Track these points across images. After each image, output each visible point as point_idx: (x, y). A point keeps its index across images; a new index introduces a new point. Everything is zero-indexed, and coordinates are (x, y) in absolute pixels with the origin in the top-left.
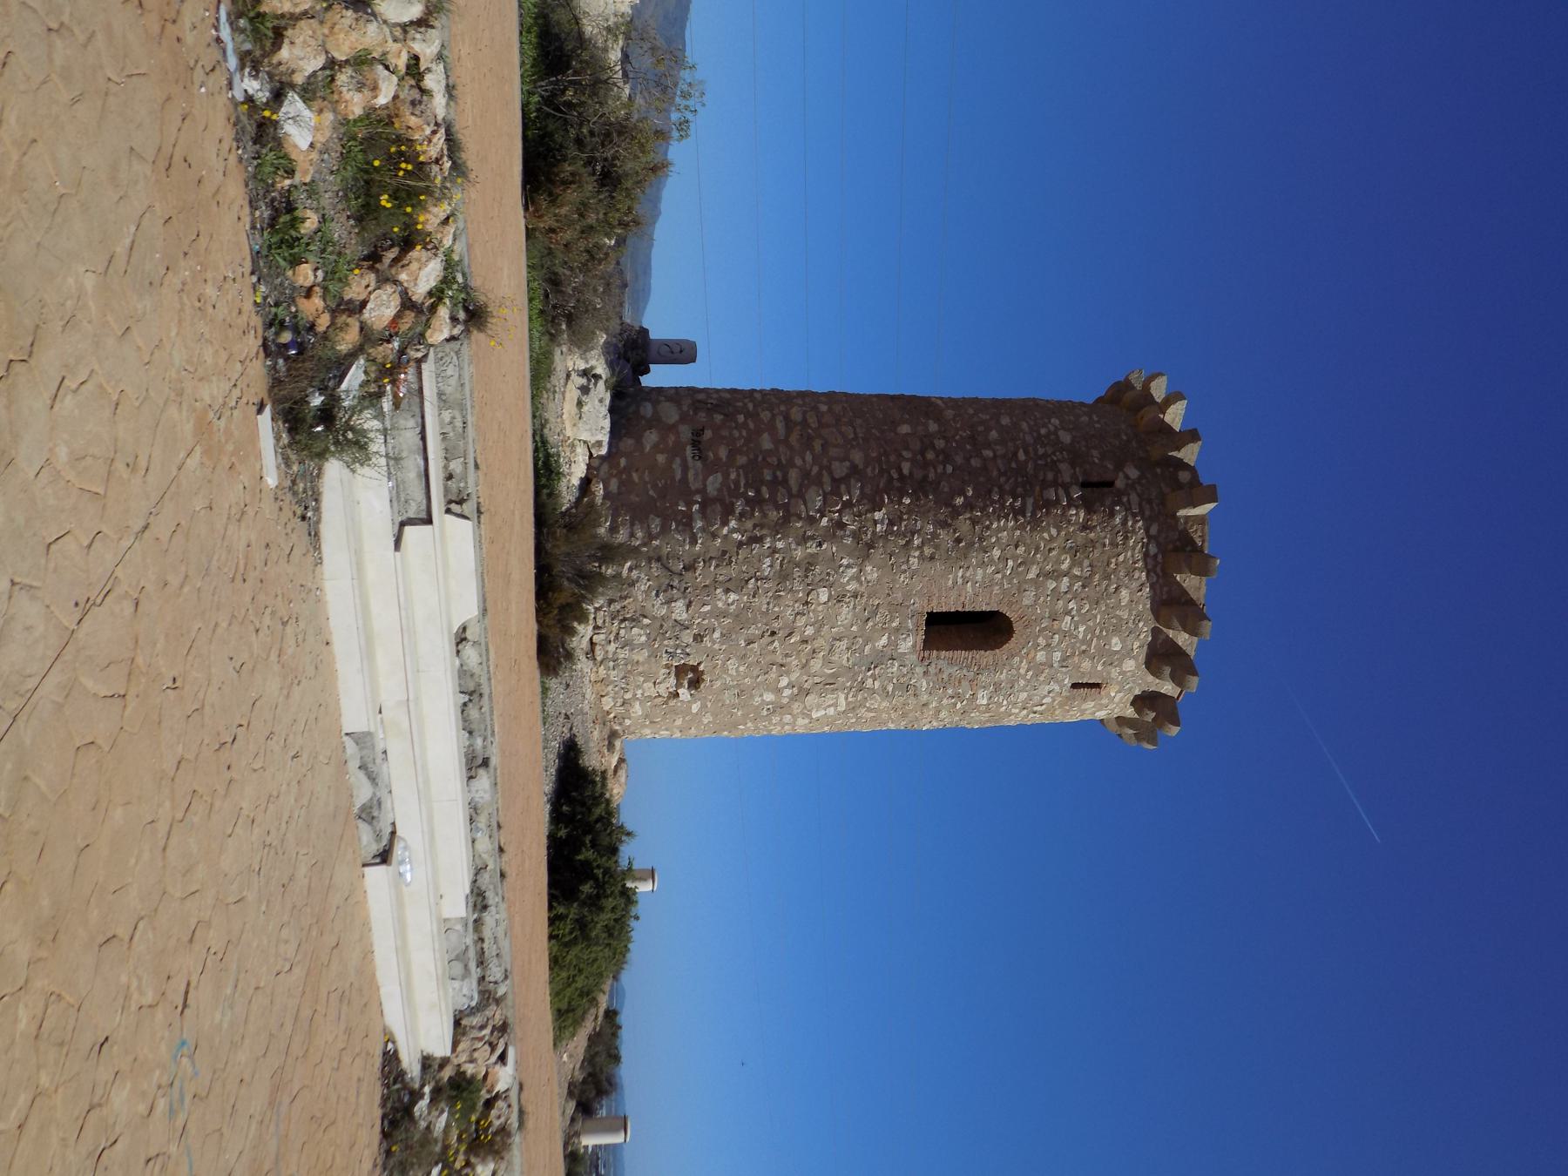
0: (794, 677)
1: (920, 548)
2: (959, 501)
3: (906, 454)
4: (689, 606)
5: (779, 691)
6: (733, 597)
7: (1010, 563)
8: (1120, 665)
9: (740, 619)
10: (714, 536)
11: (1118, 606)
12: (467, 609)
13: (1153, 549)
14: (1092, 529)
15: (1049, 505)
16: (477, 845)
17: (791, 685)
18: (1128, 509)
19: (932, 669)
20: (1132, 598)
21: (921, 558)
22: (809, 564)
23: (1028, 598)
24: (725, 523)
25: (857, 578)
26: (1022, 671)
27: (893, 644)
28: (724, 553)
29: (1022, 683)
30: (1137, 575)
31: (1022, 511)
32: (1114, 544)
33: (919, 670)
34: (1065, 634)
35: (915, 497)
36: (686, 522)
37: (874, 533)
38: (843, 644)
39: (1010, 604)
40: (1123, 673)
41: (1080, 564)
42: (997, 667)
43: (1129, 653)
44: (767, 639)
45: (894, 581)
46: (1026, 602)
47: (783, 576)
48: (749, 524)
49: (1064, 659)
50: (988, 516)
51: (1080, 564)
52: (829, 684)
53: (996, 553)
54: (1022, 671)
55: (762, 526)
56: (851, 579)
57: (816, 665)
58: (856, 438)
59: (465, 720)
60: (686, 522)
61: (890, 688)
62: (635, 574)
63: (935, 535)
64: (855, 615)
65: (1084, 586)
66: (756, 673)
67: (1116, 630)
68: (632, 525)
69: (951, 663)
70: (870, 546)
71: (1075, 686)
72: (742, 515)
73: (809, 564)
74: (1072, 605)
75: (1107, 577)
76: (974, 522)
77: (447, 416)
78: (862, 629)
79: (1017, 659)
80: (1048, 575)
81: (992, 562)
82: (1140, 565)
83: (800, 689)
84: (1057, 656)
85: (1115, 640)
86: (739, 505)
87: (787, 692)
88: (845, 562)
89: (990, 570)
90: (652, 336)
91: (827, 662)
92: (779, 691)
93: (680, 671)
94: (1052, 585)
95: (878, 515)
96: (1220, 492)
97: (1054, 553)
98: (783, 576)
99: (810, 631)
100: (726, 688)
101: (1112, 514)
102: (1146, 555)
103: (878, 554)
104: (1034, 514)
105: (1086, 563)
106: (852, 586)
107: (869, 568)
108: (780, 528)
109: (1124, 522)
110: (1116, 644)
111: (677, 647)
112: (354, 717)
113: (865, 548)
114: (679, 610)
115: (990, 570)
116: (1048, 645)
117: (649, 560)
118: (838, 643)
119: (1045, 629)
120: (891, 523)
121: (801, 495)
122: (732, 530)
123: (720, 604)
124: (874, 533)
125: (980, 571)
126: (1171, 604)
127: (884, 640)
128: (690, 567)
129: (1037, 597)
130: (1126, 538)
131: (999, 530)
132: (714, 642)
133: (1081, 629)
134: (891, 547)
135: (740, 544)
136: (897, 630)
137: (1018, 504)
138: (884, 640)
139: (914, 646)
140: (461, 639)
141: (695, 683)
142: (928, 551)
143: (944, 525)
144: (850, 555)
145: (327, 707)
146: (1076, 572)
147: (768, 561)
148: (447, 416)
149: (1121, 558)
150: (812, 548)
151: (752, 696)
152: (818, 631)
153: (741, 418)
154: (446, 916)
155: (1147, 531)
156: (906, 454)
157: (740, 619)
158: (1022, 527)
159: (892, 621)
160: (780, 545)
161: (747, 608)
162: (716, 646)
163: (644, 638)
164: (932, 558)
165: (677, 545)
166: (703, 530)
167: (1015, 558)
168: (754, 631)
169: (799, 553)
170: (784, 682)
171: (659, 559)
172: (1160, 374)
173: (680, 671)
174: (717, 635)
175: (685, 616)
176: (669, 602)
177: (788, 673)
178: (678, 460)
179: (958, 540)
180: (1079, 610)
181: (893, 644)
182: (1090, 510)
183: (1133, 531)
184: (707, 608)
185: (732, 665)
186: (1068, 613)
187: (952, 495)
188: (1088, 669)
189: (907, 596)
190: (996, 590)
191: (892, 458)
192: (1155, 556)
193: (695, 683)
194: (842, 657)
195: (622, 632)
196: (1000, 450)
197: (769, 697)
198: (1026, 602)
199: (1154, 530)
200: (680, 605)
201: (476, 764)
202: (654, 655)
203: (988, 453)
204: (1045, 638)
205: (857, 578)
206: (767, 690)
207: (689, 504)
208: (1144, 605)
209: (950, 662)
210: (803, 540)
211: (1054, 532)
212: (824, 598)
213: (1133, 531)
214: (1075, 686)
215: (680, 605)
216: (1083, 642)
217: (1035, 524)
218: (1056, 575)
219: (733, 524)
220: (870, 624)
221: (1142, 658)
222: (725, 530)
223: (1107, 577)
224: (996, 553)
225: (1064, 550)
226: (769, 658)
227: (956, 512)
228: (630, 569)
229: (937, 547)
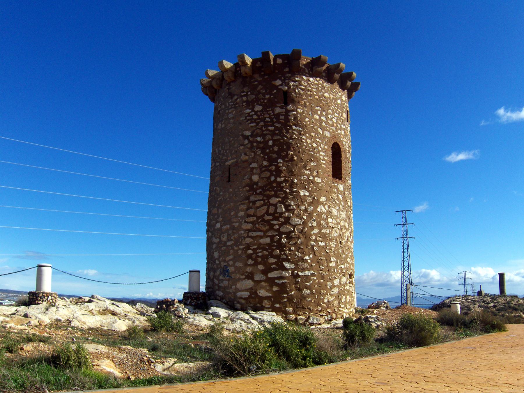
3: (273, 179)
7: (317, 140)
11: (329, 98)
14: (305, 103)
23: (327, 134)
32: (310, 96)
48: (306, 250)
53: (314, 145)
58: (264, 200)
65: (324, 111)
75: (321, 101)
90: (187, 291)
95: (302, 194)
96: (265, 50)
105: (317, 108)
106: (326, 207)
108: (307, 237)
120: (305, 188)
121: (294, 226)
125: (321, 153)
130: (309, 90)
131: (306, 142)
135: (315, 255)
137: (296, 133)
146: (319, 113)
147: (320, 243)
153: (250, 252)
156: (273, 179)
157: (338, 256)
159: (335, 192)
172: (221, 63)
178: (277, 281)
191: (274, 185)
196: (268, 137)
203: (270, 143)
219: (307, 258)
222: (309, 261)
223: (321, 101)
224: (314, 145)
227: (301, 160)
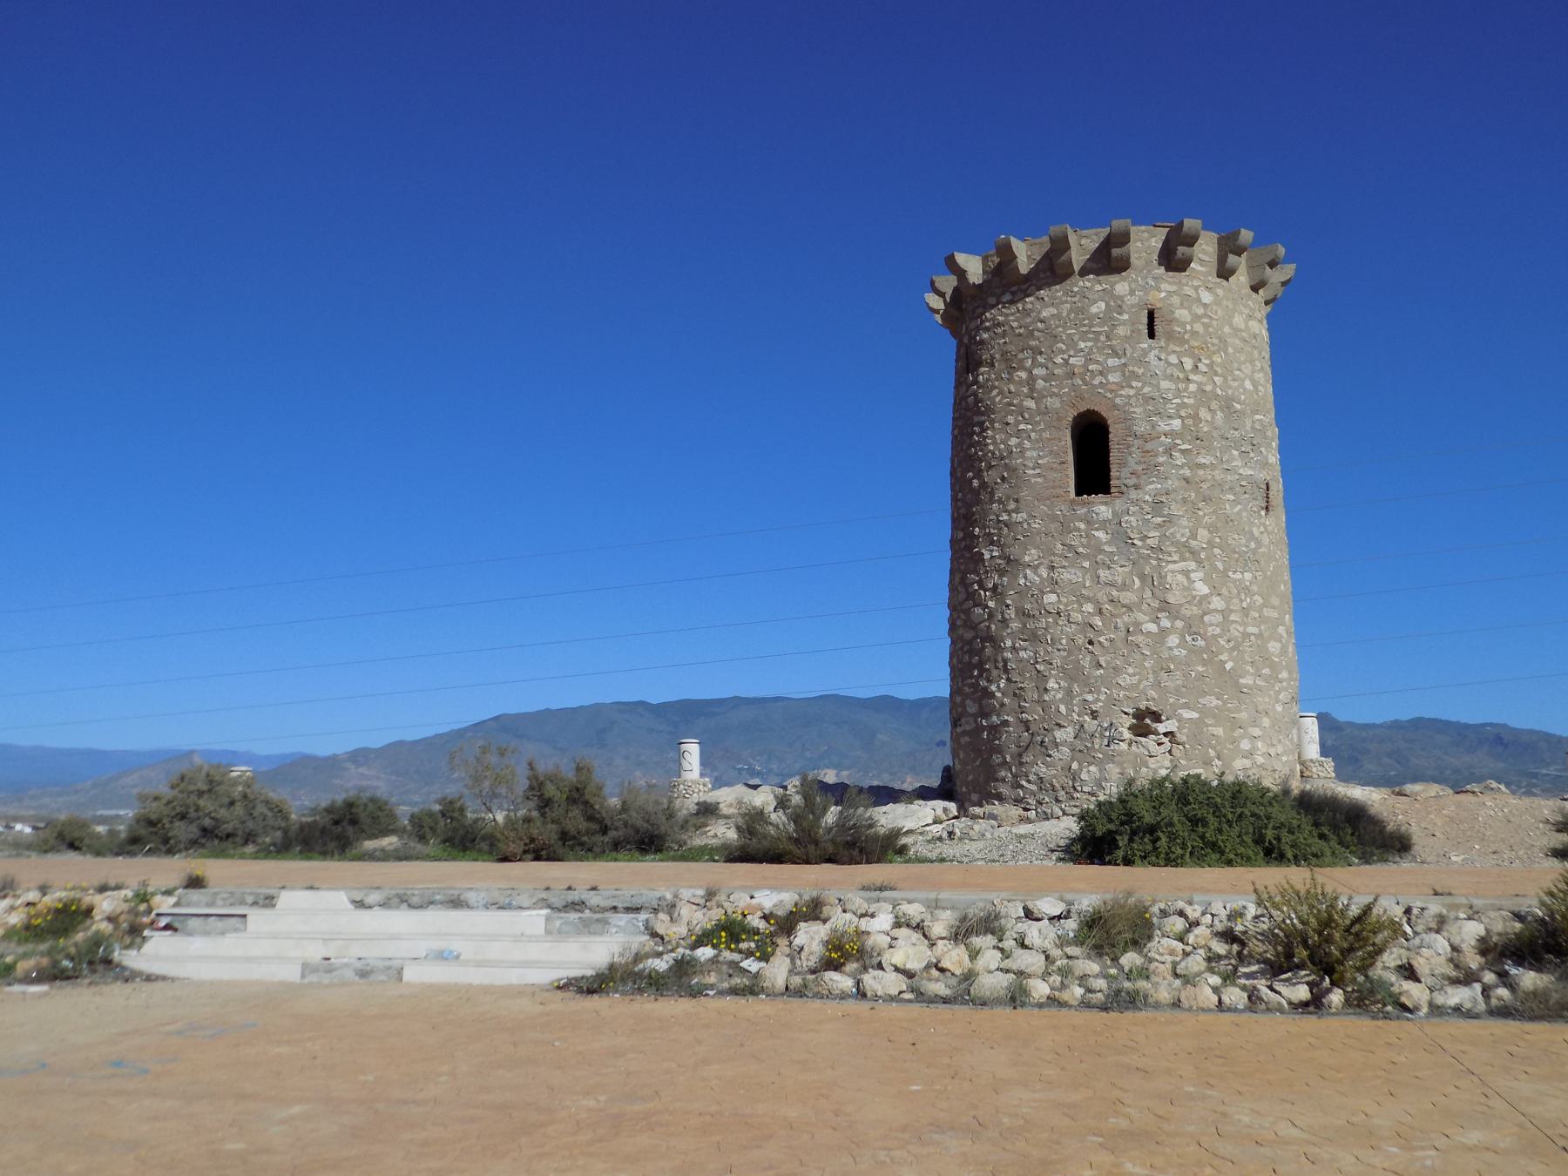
0: (1141, 617)
1: (1009, 513)
2: (976, 483)
4: (1060, 726)
5: (1164, 632)
6: (1052, 684)
7: (1022, 427)
8: (1121, 298)
9: (1073, 675)
10: (1003, 705)
11: (1058, 317)
12: (341, 898)
13: (1007, 297)
14: (992, 357)
15: (978, 400)
16: (525, 904)
17: (1156, 620)
18: (978, 329)
19: (1131, 482)
20: (1050, 305)
21: (1017, 511)
22: (1023, 614)
23: (1053, 403)
24: (992, 695)
25: (1035, 568)
26: (1132, 392)
27: (1104, 525)
28: (1015, 694)
29: (1146, 389)
30: (1029, 306)
31: (981, 424)
32: (1004, 334)
33: (1133, 494)
34: (1089, 360)
35: (974, 523)
36: (994, 729)
37: (999, 557)
38: (1104, 574)
39: (1060, 419)
40: (1132, 293)
41: (1022, 361)
42: (1128, 419)
43: (1108, 294)
44: (1096, 649)
45: (1038, 533)
46: (1058, 405)
47: (1034, 638)
48: (995, 673)
49: (1116, 354)
50: (985, 455)
51: (1022, 361)
52: (1155, 583)
54: (1132, 392)
55: (996, 661)
56: (1036, 573)
57: (1127, 597)
59: (421, 907)
60: (994, 729)
61: (1159, 520)
62: (1031, 777)
63: (1000, 501)
64: (1072, 566)
66: (1138, 656)
67: (1082, 310)
68: (997, 780)
69: (1122, 465)
70: (1008, 560)
71: (1152, 335)
72: (989, 681)
73: (1023, 614)
74: (1059, 360)
76: (990, 467)
77: (220, 902)
78: (1086, 557)
79: (1118, 401)
80: (1032, 390)
81: (1019, 445)
82: (1020, 306)
83: (1161, 610)
84: (1112, 362)
85: (1094, 310)
86: (983, 683)
87: (1166, 623)
88: (1022, 582)
89: (1027, 444)
91: (1124, 587)
92: (1164, 632)
93: (1141, 730)
94: (1040, 383)
95: (987, 556)
97: (1012, 388)
98: (1034, 638)
99: (1089, 608)
100: (1157, 685)
101: (982, 342)
102: (1012, 302)
103: (1014, 552)
104: (983, 414)
105: (1020, 356)
106: (1044, 572)
107: (1027, 558)
108: (998, 649)
109: (987, 329)
110: (1099, 307)
111: (1102, 736)
112: (291, 973)
113: (1011, 564)
114: (1065, 735)
115: (1027, 444)
116: (1101, 373)
117: (1021, 764)
118: (1102, 579)
119: (1083, 380)
120: (992, 543)
122: (998, 687)
123: (1059, 696)
124: (999, 557)
125: (1028, 454)
126: (1053, 269)
127: (1101, 535)
128: (1026, 725)
129: (1053, 395)
130: (999, 325)
131: (995, 443)
132: (1097, 700)
133: (1082, 345)
134: (1010, 540)
135: (1009, 680)
136: (1089, 523)
138: (1101, 535)
139: (1106, 504)
140: (360, 904)
141: (1157, 717)
142: (1012, 506)
143: (992, 494)
144: (1016, 577)
145: (288, 986)
147: (1022, 654)
148: (220, 902)
149: (1015, 324)
150: (1011, 613)
151: (1172, 659)
152: (1088, 599)
154: (542, 931)
155: (993, 307)
157: (1073, 675)
158: (992, 422)
159: (1079, 530)
160: (1009, 643)
161: (1063, 670)
162: (1102, 697)
163: (1092, 768)
164: (1017, 501)
165: (1011, 737)
166: (998, 715)
167: (1018, 423)
168: (1086, 662)
169: (1015, 625)
170: (1152, 627)
171: (1020, 755)
173: (1141, 730)
174: (1089, 697)
175: (1070, 729)
176: (1056, 745)
177: (1138, 624)
179: (1003, 479)
180: (1063, 352)
181: (1104, 525)
182: (980, 364)
183: (993, 319)
184: (1063, 708)
185: (1125, 680)
186: (1066, 361)
187: (972, 489)
188: (1129, 324)
189: (1054, 518)
190: (1046, 435)
192: (1013, 293)
193: (1157, 717)
194: (1120, 573)
195: (1086, 789)
197: (1173, 640)
198: (1058, 405)
199: (992, 300)
200: (1059, 735)
201: (456, 903)
202: (1111, 758)
204: (1093, 378)
205: (1035, 568)
206: (1162, 643)
207: (983, 728)
208: (1058, 291)
209: (1123, 463)
210: (1005, 622)
211: (995, 392)
212: (1053, 598)
213: (993, 319)
214: (1152, 335)
215: (1059, 735)
216: (1096, 340)
217: (989, 410)
218: (1032, 379)
219: (993, 688)
220: (1081, 550)
221: (1113, 278)
222: (998, 695)
225: (1010, 380)
226: (1119, 644)
227: (984, 485)
228: (1029, 782)
229: (1008, 498)
